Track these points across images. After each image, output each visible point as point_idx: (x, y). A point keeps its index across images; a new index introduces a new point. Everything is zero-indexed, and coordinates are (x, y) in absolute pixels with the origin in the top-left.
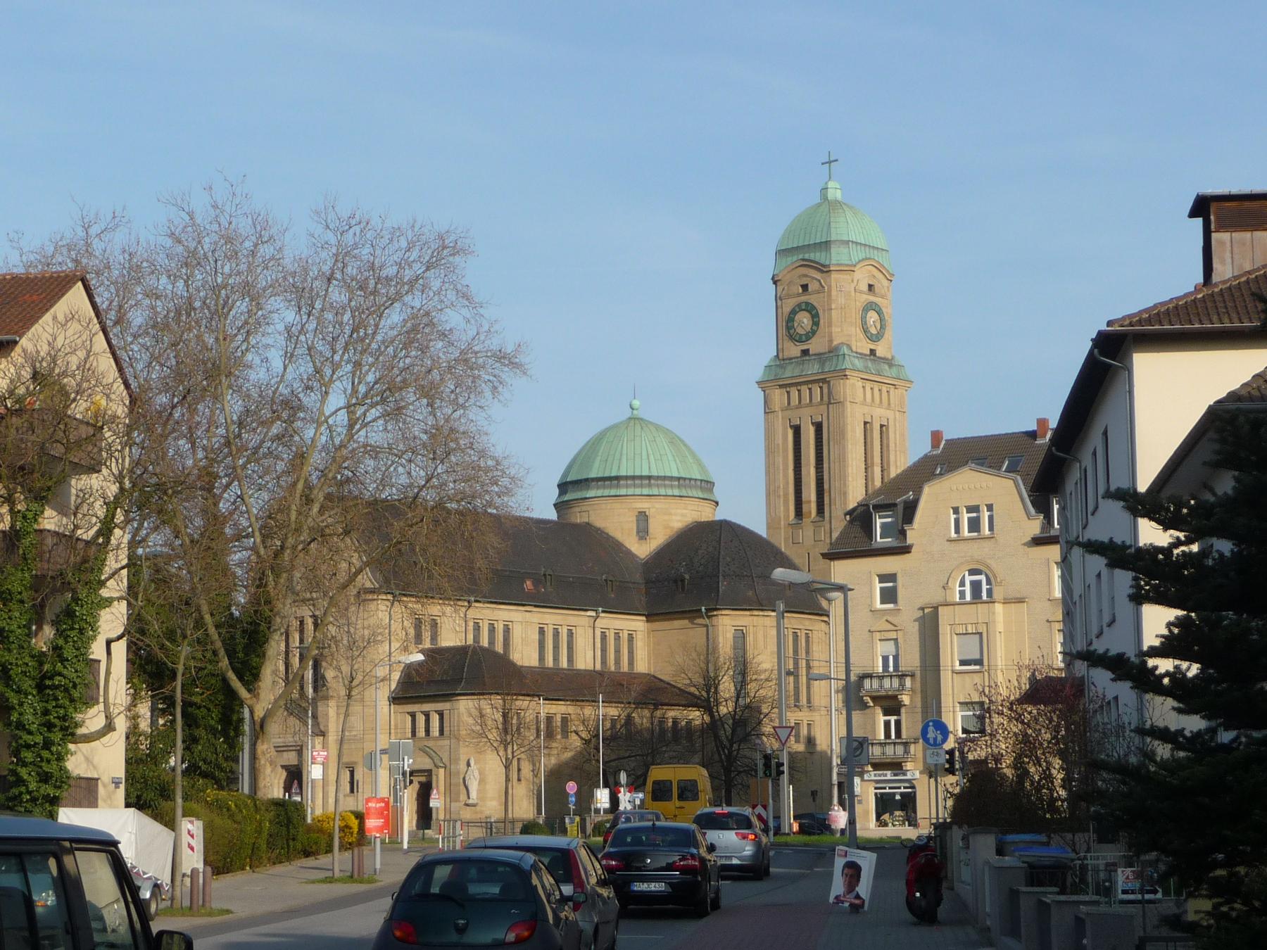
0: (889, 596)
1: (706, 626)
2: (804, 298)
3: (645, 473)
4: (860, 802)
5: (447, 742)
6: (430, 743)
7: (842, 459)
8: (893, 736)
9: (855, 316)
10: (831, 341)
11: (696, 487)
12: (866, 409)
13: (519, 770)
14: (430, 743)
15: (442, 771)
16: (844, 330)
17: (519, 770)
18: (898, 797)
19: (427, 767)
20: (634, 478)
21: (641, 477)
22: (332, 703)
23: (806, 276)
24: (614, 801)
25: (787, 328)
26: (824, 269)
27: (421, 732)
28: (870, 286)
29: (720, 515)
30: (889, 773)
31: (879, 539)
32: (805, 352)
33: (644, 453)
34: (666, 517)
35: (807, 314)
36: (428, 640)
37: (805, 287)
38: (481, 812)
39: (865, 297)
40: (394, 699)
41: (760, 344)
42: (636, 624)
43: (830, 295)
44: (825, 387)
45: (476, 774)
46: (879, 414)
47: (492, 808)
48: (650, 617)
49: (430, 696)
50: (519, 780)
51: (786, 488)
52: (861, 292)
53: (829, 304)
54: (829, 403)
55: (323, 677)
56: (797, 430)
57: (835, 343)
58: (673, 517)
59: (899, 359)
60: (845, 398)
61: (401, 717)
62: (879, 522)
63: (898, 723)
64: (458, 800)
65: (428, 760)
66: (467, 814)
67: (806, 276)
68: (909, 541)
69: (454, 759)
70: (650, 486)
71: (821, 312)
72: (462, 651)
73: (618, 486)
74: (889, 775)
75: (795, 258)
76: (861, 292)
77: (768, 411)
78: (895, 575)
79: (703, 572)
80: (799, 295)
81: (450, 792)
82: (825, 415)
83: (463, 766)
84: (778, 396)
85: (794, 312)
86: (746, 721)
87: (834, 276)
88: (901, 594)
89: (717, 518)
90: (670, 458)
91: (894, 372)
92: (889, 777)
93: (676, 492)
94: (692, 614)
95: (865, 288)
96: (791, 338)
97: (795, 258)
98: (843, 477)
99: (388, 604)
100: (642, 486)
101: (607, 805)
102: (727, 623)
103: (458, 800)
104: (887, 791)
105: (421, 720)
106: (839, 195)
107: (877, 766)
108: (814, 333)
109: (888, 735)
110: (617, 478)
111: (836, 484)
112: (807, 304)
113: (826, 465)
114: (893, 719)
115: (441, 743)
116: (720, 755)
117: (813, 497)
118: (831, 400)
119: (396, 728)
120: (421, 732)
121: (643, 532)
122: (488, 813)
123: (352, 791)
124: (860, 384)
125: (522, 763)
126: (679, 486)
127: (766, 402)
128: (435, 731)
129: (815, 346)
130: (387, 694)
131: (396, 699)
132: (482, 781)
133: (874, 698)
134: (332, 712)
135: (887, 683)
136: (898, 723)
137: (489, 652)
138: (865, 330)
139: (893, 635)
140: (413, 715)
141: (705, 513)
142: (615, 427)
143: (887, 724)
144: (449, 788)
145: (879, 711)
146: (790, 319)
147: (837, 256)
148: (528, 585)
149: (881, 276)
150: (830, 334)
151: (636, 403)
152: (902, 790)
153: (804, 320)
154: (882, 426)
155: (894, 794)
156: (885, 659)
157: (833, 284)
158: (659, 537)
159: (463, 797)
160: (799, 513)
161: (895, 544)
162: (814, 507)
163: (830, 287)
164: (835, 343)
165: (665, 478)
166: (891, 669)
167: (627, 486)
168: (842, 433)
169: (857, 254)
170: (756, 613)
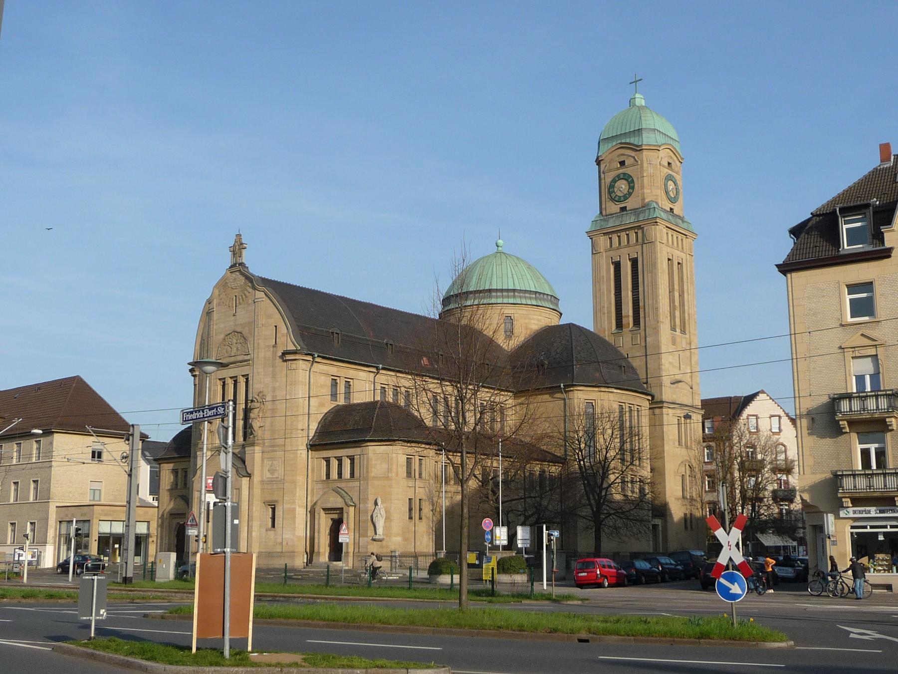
0: (863, 308)
1: (564, 399)
2: (621, 171)
3: (511, 287)
4: (834, 543)
5: (357, 484)
6: (342, 485)
7: (654, 285)
8: (874, 466)
9: (660, 182)
10: (644, 199)
11: (547, 300)
12: (669, 249)
13: (420, 510)
14: (342, 485)
15: (352, 509)
16: (652, 191)
17: (420, 510)
18: (881, 538)
19: (339, 506)
20: (502, 290)
21: (508, 290)
22: (257, 449)
23: (623, 155)
24: (512, 537)
25: (608, 192)
26: (638, 149)
27: (334, 474)
28: (669, 164)
29: (564, 321)
30: (873, 509)
31: (846, 247)
32: (623, 209)
33: (510, 275)
34: (526, 321)
35: (624, 182)
36: (343, 396)
37: (622, 163)
38: (387, 547)
39: (666, 170)
40: (311, 445)
41: (587, 207)
42: (507, 399)
43: (642, 167)
44: (640, 232)
45: (383, 512)
46: (677, 255)
47: (396, 543)
48: (517, 394)
49: (343, 443)
50: (420, 518)
51: (609, 312)
52: (664, 166)
53: (642, 173)
54: (643, 243)
55: (251, 427)
56: (617, 266)
57: (646, 201)
58: (531, 321)
59: (687, 219)
60: (656, 240)
61: (317, 461)
62: (844, 228)
63: (881, 454)
64: (366, 536)
65: (339, 500)
66: (374, 548)
67: (623, 155)
68: (887, 245)
69: (363, 498)
70: (514, 297)
71: (635, 180)
72: (372, 406)
73: (490, 297)
74: (873, 512)
75: (610, 145)
76: (664, 166)
77: (595, 252)
78: (871, 283)
79: (557, 360)
80: (618, 169)
81: (359, 528)
82: (640, 253)
83: (370, 505)
84: (603, 242)
85: (614, 181)
86: (594, 478)
87: (645, 153)
88: (881, 305)
89: (561, 323)
90: (529, 277)
91: (685, 226)
92: (873, 514)
93: (534, 303)
94: (553, 390)
95: (666, 164)
96: (613, 200)
97: (614, 143)
98: (655, 297)
99: (309, 364)
100: (508, 297)
101: (505, 543)
102: (581, 396)
103: (366, 536)
104: (869, 530)
105: (334, 464)
106: (643, 103)
107: (857, 501)
108: (630, 194)
109: (866, 463)
110: (490, 291)
111: (649, 302)
112: (624, 174)
113: (641, 289)
114: (873, 447)
115: (351, 484)
116: (589, 499)
117: (631, 313)
118: (645, 241)
119: (313, 470)
120: (334, 474)
121: (510, 334)
122: (392, 547)
123: (273, 526)
124: (665, 230)
125: (423, 503)
126: (536, 299)
127: (593, 246)
128: (347, 473)
129: (630, 204)
130: (305, 441)
131: (314, 446)
132: (388, 519)
133: (851, 423)
134: (258, 456)
135: (871, 404)
136: (881, 454)
137: (395, 406)
138: (667, 193)
139: (872, 351)
140: (328, 460)
141: (555, 321)
142: (488, 257)
143: (865, 453)
144: (358, 523)
145: (854, 437)
146: (612, 186)
147: (647, 139)
148: (425, 361)
149: (675, 158)
150: (643, 194)
151: (501, 242)
152: (889, 530)
153: (622, 186)
154: (679, 263)
155: (877, 534)
156: (860, 379)
157: (645, 159)
158: (521, 335)
159: (371, 533)
160: (619, 324)
161: (870, 248)
162: (631, 319)
163: (642, 161)
164: (646, 201)
165: (525, 291)
166: (868, 388)
167: (497, 297)
168: (654, 264)
169: (661, 140)
170: (603, 389)
